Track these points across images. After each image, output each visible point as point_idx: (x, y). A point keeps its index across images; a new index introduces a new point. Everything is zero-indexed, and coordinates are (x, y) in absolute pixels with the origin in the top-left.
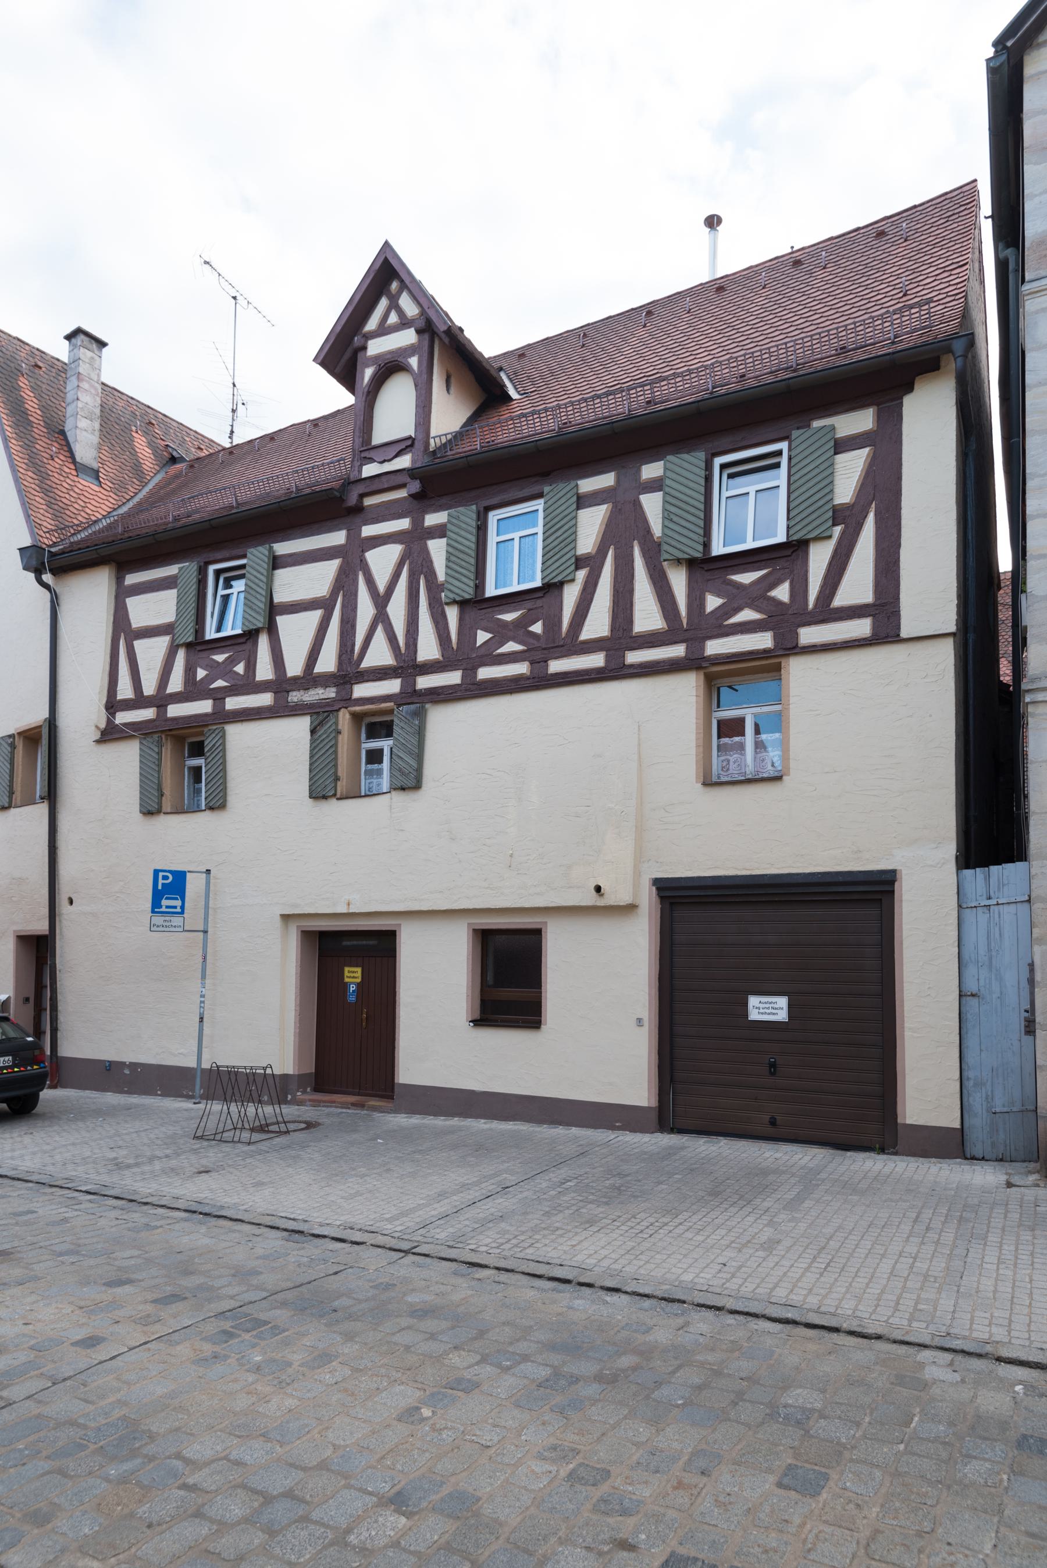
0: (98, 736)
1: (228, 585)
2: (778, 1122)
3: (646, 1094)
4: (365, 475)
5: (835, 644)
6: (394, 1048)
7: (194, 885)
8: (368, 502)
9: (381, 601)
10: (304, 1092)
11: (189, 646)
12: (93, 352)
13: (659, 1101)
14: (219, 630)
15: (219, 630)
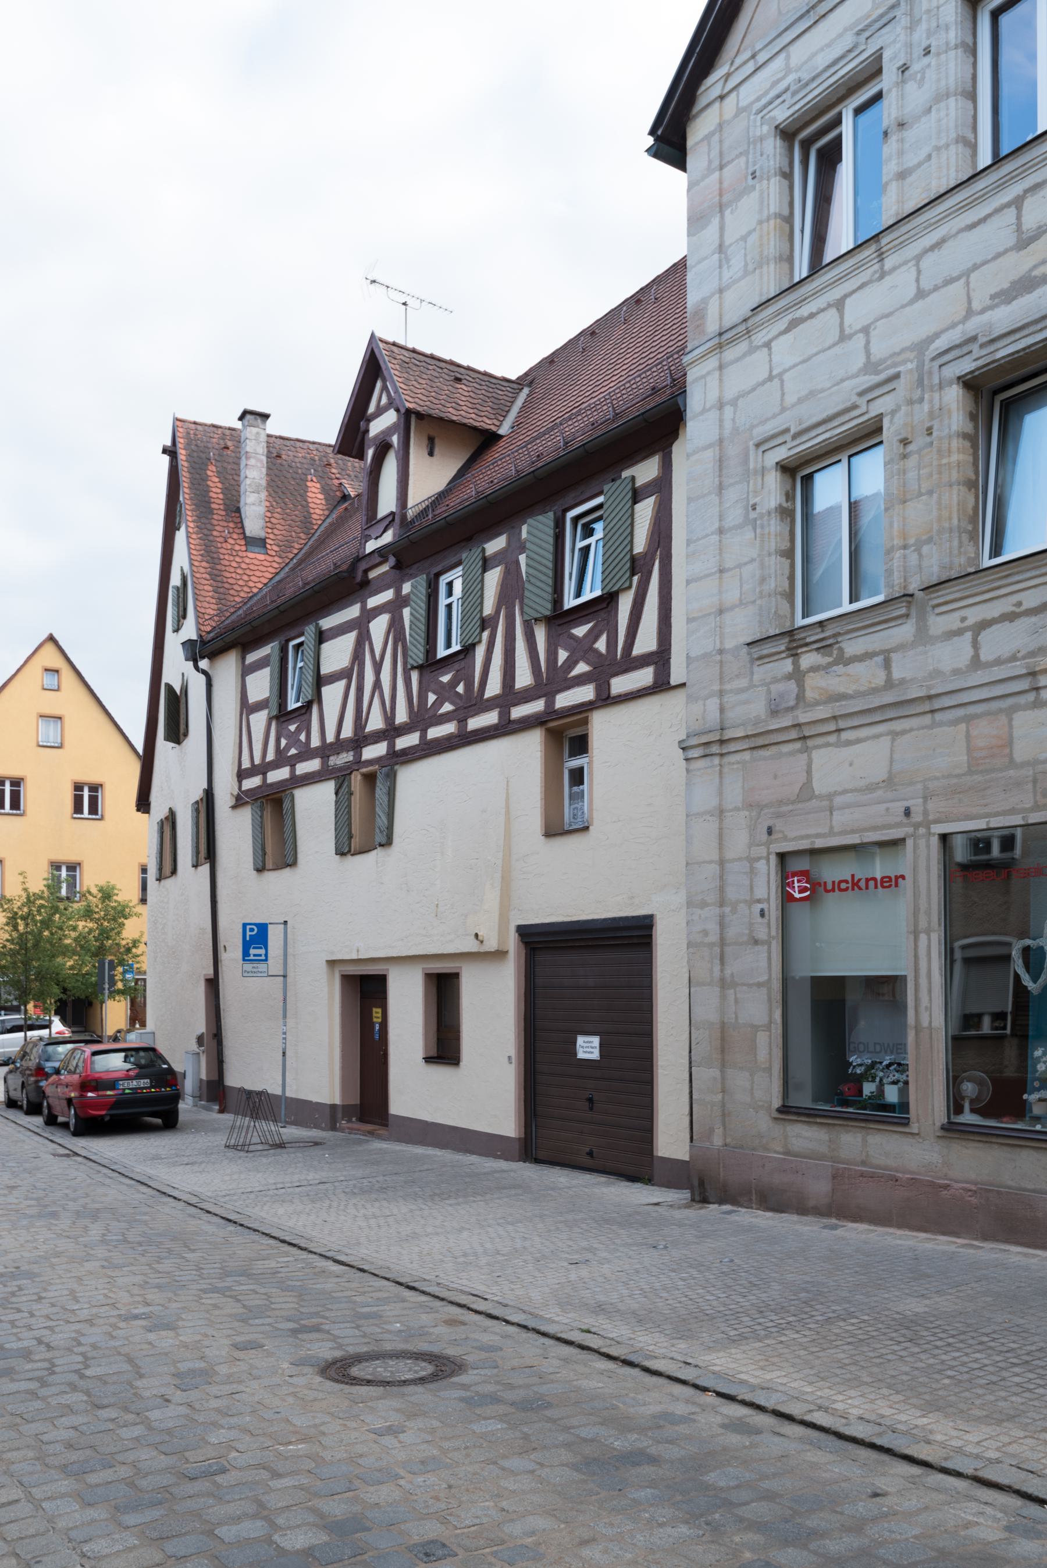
0: (232, 802)
1: (588, 532)
2: (595, 1155)
3: (513, 1126)
4: (367, 551)
5: (632, 693)
6: (525, 1101)
7: (275, 936)
8: (372, 575)
9: (378, 667)
10: (349, 1121)
11: (420, 668)
12: (258, 427)
13: (525, 1133)
14: (578, 594)
15: (578, 594)
